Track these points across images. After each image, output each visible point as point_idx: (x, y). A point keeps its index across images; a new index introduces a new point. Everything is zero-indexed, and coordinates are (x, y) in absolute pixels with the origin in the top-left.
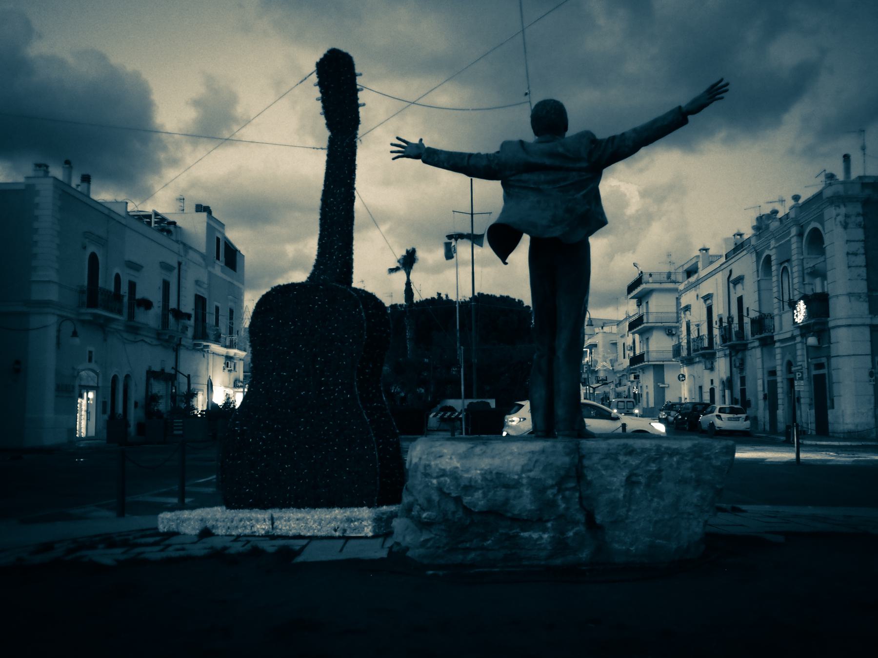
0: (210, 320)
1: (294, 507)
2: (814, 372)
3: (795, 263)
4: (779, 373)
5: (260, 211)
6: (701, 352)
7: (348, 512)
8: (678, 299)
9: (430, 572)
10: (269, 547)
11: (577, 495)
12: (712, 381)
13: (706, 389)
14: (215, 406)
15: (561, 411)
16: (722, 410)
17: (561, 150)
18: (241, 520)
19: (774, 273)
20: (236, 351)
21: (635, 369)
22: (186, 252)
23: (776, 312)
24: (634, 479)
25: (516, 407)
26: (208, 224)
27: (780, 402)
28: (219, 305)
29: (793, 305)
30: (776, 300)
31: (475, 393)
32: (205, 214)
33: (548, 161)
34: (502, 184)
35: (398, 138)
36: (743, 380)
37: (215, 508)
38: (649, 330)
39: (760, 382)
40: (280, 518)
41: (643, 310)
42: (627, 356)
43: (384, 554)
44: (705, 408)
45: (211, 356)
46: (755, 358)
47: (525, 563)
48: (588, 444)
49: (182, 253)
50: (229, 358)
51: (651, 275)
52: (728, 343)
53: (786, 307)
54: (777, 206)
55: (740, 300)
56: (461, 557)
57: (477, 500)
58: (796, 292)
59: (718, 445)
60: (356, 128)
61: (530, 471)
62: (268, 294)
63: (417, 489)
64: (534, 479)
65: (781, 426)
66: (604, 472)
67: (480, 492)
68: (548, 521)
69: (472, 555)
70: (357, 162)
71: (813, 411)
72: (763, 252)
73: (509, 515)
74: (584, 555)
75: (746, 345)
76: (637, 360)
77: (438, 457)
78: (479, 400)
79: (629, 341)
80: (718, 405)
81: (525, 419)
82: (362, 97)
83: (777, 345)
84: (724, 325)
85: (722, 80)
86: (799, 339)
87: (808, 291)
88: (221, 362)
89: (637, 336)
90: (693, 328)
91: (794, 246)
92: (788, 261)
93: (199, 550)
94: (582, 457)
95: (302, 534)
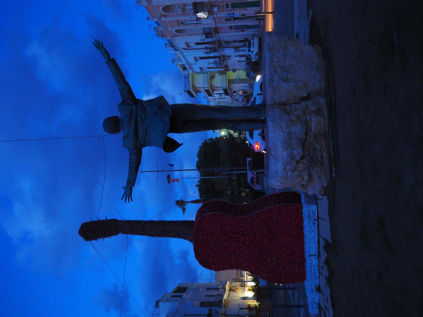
0: (211, 299)
1: (303, 246)
2: (230, 8)
3: (179, 18)
4: (231, 25)
5: (158, 276)
6: (222, 62)
7: (305, 217)
8: (197, 73)
9: (334, 174)
10: (324, 255)
11: (293, 105)
12: (235, 56)
13: (239, 59)
14: (254, 296)
15: (252, 116)
16: (249, 51)
17: (127, 119)
18: (312, 272)
19: (184, 28)
20: (227, 286)
21: (231, 93)
23: (202, 27)
24: (285, 78)
25: (251, 146)
26: (165, 301)
27: (244, 24)
28: (204, 295)
29: (199, 19)
30: (197, 27)
31: (245, 168)
32: (160, 303)
33: (133, 125)
34: (143, 147)
35: (122, 199)
36: (235, 42)
37: (306, 286)
38: (211, 86)
39: (235, 34)
40: (310, 252)
41: (202, 90)
42: (224, 97)
43: (325, 198)
44: (248, 58)
45: (230, 299)
46: (224, 36)
47: (327, 129)
48: (269, 101)
50: (230, 290)
51: (186, 87)
52: (217, 49)
53: (199, 22)
54: (153, 27)
55: (197, 44)
56: (325, 160)
57: (298, 152)
58: (193, 17)
59: (267, 40)
60: (118, 220)
61: (282, 127)
62: (199, 262)
63: (293, 183)
64: (286, 126)
65: (257, 23)
66: (282, 93)
67: (293, 151)
68: (306, 119)
69: (324, 155)
70: (134, 220)
71: (249, 8)
72: (173, 34)
73: (304, 137)
74: (322, 101)
75: (218, 41)
76: (226, 92)
77: (278, 178)
78: (248, 166)
79: (217, 96)
80: (247, 53)
81: (256, 142)
82: (102, 218)
83: (217, 26)
84: (209, 51)
85: (93, 43)
86: (215, 16)
87: (192, 12)
88: (233, 294)
89: (215, 92)
90: (211, 66)
91: (171, 19)
92: (178, 22)
93: (327, 291)
94: (275, 103)
95: (317, 240)
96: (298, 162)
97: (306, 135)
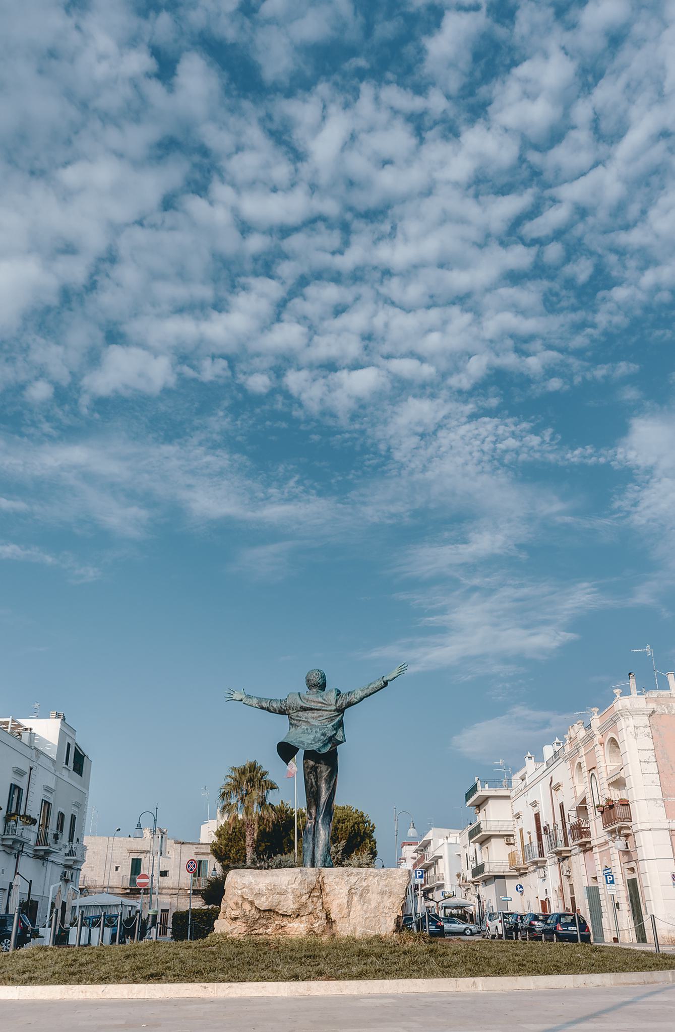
22: (38, 757)
24: (353, 891)
28: (62, 810)
49: (34, 758)
55: (562, 806)
57: (263, 903)
73: (281, 912)
83: (595, 850)
96: (252, 903)
97: (283, 915)
